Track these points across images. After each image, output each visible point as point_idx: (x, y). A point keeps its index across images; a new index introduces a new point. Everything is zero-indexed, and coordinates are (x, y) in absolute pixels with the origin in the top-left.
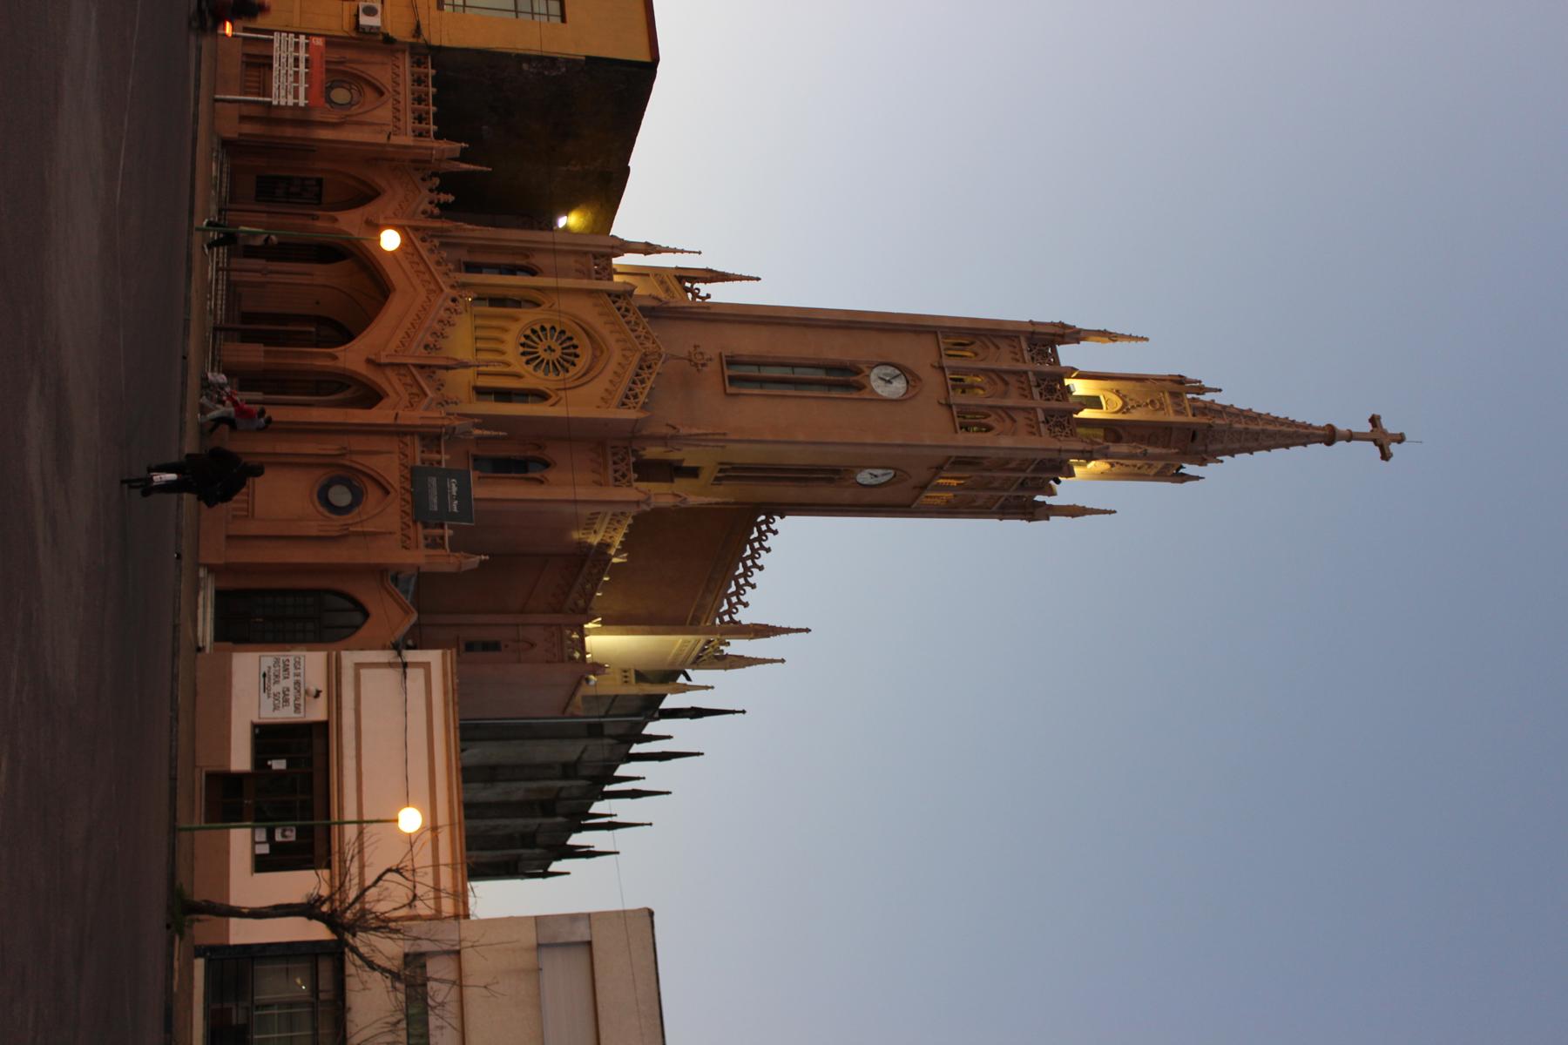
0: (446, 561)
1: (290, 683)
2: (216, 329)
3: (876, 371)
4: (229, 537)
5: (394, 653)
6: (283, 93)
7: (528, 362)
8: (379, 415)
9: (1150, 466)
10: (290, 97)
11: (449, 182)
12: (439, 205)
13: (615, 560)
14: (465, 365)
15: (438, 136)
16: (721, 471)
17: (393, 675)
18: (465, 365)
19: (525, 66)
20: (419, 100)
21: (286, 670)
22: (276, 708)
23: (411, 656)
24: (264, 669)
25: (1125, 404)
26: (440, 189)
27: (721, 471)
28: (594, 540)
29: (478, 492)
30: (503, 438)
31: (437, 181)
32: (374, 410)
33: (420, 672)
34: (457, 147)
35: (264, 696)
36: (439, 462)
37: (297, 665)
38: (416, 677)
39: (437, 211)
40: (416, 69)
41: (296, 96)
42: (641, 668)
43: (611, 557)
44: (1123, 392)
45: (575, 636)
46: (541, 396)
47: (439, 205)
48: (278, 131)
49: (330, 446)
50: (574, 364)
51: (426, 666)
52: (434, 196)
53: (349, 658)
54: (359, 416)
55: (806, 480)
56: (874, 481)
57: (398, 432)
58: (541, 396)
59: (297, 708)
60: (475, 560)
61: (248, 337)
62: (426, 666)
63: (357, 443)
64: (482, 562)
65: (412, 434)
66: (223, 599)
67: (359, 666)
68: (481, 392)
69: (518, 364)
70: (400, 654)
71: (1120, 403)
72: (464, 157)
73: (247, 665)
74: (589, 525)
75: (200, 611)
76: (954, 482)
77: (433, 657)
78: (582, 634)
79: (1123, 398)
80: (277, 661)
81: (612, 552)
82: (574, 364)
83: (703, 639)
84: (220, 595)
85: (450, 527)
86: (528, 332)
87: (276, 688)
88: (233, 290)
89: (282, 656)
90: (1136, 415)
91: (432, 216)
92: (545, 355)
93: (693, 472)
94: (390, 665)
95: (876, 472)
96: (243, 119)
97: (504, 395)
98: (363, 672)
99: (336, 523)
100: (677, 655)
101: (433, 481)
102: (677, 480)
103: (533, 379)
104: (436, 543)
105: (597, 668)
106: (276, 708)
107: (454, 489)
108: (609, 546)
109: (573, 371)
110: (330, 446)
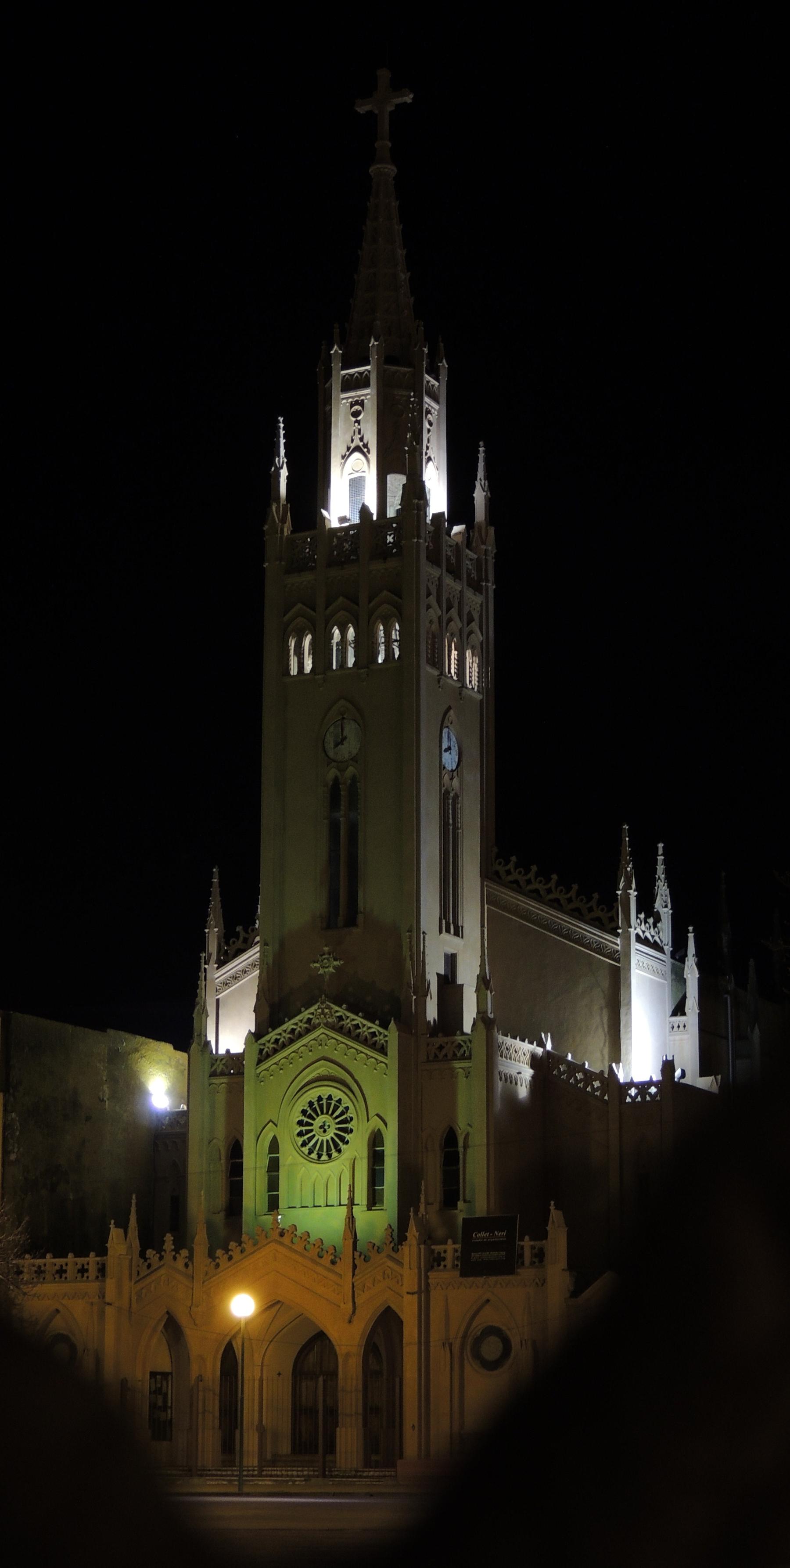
2: (324, 1476)
11: (149, 1240)
12: (177, 1250)
13: (549, 1046)
16: (448, 931)
19: (13, 1157)
20: (61, 1271)
25: (357, 449)
27: (448, 931)
28: (528, 1073)
32: (403, 1317)
34: (115, 1233)
36: (456, 1251)
39: (184, 1253)
40: (48, 1276)
42: (669, 1008)
44: (343, 450)
45: (633, 1091)
46: (376, 1140)
47: (177, 1250)
48: (200, 1416)
49: (440, 1357)
52: (168, 1256)
55: (455, 828)
57: (424, 1291)
58: (376, 1140)
60: (555, 1215)
63: (436, 1336)
64: (557, 1208)
65: (427, 1277)
69: (338, 1166)
71: (357, 455)
72: (123, 1225)
74: (510, 1081)
76: (454, 653)
81: (540, 1051)
82: (339, 1101)
85: (522, 1239)
88: (270, 1461)
90: (371, 437)
91: (191, 1257)
92: (331, 1134)
100: (654, 972)
101: (475, 1256)
103: (356, 1147)
104: (540, 1256)
108: (534, 1057)
110: (440, 1357)
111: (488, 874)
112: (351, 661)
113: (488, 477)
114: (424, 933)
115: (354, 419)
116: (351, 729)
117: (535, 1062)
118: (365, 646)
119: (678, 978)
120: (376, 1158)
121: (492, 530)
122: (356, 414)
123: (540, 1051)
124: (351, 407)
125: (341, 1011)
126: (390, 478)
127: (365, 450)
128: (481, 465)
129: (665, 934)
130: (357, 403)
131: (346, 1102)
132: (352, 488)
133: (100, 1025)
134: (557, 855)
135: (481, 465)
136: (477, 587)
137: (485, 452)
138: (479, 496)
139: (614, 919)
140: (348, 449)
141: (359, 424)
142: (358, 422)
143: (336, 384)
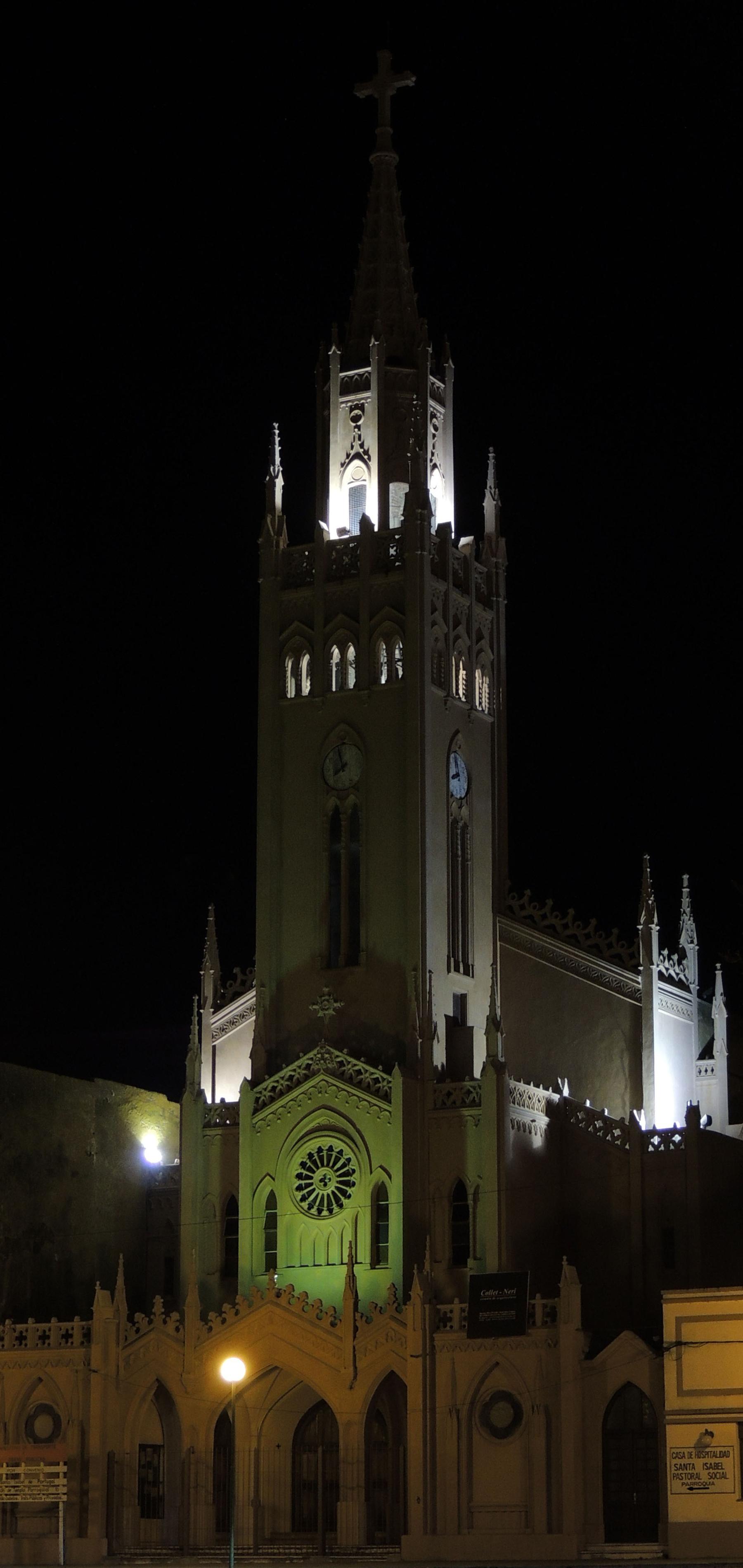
0: (571, 1295)
1: (699, 1463)
3: (331, 782)
4: (550, 1531)
5: (666, 1354)
6: (52, 1490)
7: (341, 1206)
8: (413, 1377)
9: (433, 416)
10: (56, 1482)
11: (138, 1303)
12: (167, 1313)
13: (566, 1092)
14: (351, 1278)
15: (88, 1315)
16: (457, 970)
17: (690, 1356)
18: (351, 1278)
21: (685, 1467)
22: (724, 1476)
23: (669, 1334)
24: (685, 1489)
25: (358, 456)
26: (148, 1313)
28: (543, 1121)
29: (492, 1264)
30: (430, 1237)
31: (138, 1316)
33: (686, 1328)
34: (101, 1295)
35: (712, 1489)
37: (677, 1456)
38: (689, 1332)
39: (175, 1316)
41: (57, 1475)
42: (696, 1051)
43: (564, 1100)
44: (343, 458)
45: (656, 1140)
46: (380, 1194)
47: (167, 1313)
50: (341, 1152)
51: (680, 1321)
52: (158, 1320)
53: (672, 1401)
54: (415, 1397)
55: (465, 860)
56: (464, 776)
57: (429, 1354)
59: (724, 1455)
60: (568, 1271)
61: (331, 1523)
62: (680, 1321)
66: (614, 1535)
67: (681, 1393)
68: (378, 1258)
69: (341, 1220)
70: (668, 1349)
71: (357, 463)
72: (109, 1285)
73: (683, 1507)
74: (524, 1130)
75: (625, 1556)
76: (462, 673)
77: (671, 1311)
78: (653, 1132)
79: (351, 458)
80: (675, 1476)
81: (556, 1097)
83: (657, 984)
84: (608, 1540)
86: (305, 1205)
87: (704, 1477)
89: (671, 1470)
92: (332, 1187)
93: (461, 1001)
94: (679, 1359)
95: (453, 772)
96: (82, 1533)
97: (379, 1233)
98: (685, 1388)
99: (72, 1435)
102: (470, 1023)
103: (359, 1200)
104: (552, 1315)
105: (693, 1113)
106: (724, 1476)
107: (490, 1293)
109: (338, 1145)
111: (501, 908)
112: (351, 681)
113: (497, 485)
114: (430, 971)
115: (354, 424)
116: (350, 755)
117: (550, 1109)
118: (367, 667)
119: (706, 1019)
120: (380, 1213)
121: (502, 542)
122: (355, 419)
123: (556, 1097)
124: (351, 412)
125: (342, 1057)
126: (392, 486)
127: (366, 457)
128: (491, 472)
129: (691, 971)
130: (357, 407)
131: (348, 1153)
132: (351, 497)
133: (88, 1074)
134: (577, 889)
135: (491, 472)
136: (486, 602)
137: (494, 458)
138: (489, 505)
139: (634, 956)
140: (348, 456)
141: (359, 430)
142: (358, 427)
143: (334, 388)
